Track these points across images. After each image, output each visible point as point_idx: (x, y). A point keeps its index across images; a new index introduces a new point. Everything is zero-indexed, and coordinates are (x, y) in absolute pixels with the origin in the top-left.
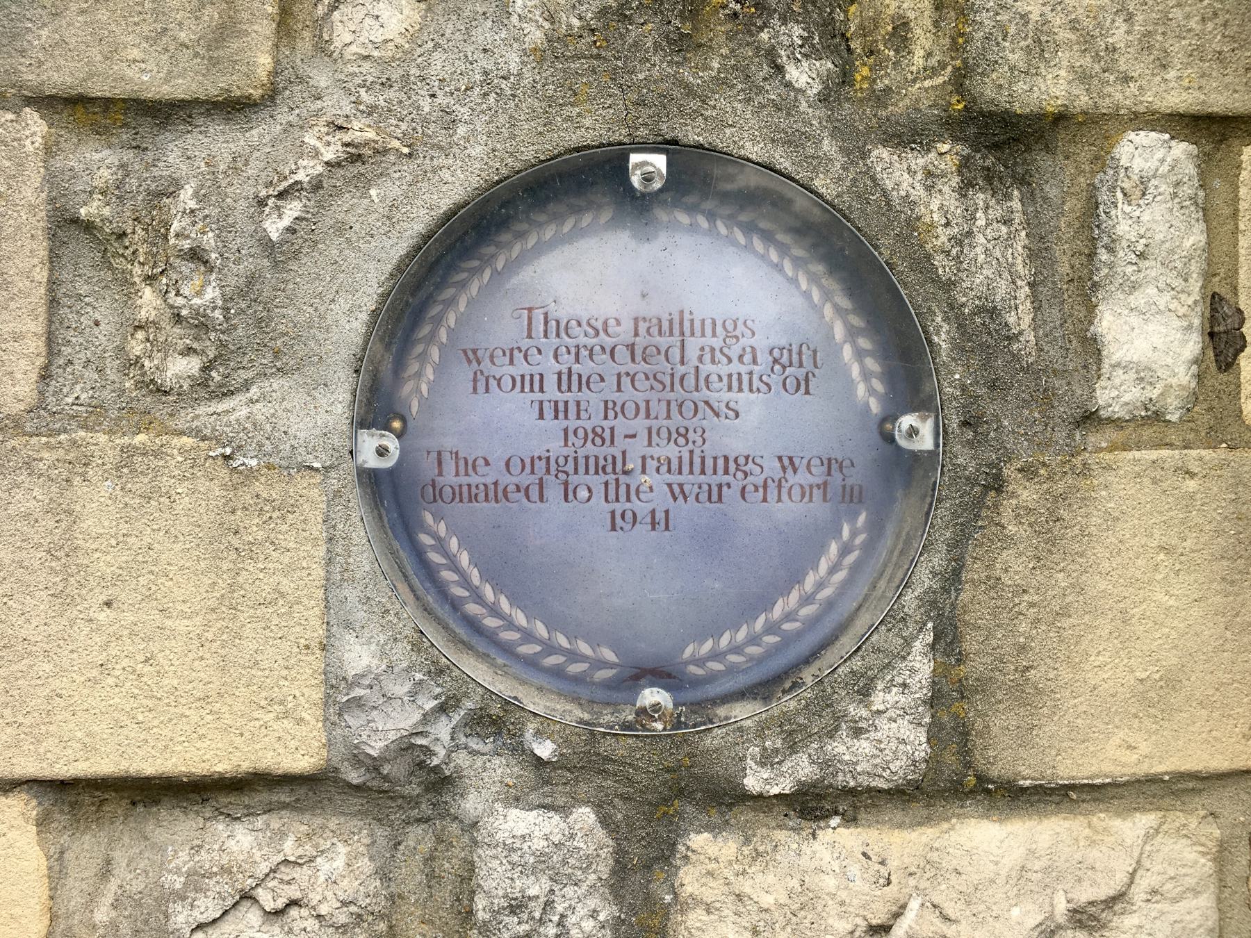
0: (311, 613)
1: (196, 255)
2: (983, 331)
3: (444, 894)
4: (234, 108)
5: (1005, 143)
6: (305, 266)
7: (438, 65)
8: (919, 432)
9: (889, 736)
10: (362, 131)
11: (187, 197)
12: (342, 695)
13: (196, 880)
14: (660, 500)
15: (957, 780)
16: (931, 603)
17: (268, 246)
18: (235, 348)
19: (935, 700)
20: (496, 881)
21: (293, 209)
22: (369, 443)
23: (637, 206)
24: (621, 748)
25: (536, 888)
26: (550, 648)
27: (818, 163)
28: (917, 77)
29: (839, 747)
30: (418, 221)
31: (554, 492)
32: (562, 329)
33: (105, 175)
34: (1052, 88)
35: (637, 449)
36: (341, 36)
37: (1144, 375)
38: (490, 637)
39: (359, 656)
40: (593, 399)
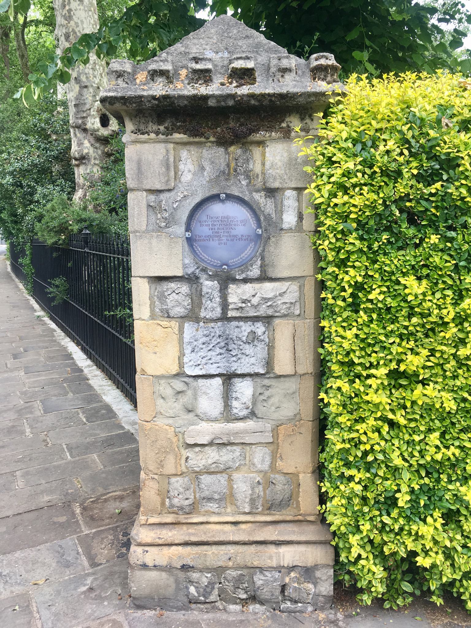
0: (181, 255)
1: (165, 210)
2: (268, 218)
3: (198, 293)
4: (169, 190)
5: (271, 192)
6: (179, 211)
7: (195, 183)
8: (260, 231)
9: (255, 272)
10: (186, 193)
11: (164, 202)
12: (185, 266)
13: (168, 289)
14: (225, 241)
15: (264, 278)
16: (260, 254)
17: (174, 208)
18: (170, 222)
19: (261, 267)
20: (205, 290)
21: (177, 204)
22: (187, 234)
23: (222, 201)
24: (220, 273)
25: (210, 291)
26: (211, 261)
27: (245, 195)
28: (259, 183)
29: (249, 273)
30: (193, 205)
31: (211, 240)
32: (212, 218)
33: (153, 199)
34: (276, 185)
35: (222, 234)
36: (182, 180)
37: (289, 224)
38: (203, 260)
39: (187, 261)
40: (216, 227)
